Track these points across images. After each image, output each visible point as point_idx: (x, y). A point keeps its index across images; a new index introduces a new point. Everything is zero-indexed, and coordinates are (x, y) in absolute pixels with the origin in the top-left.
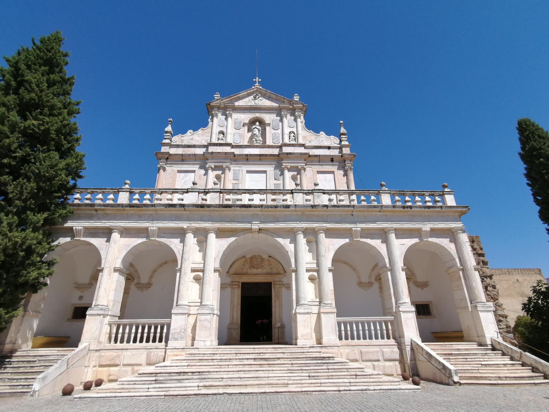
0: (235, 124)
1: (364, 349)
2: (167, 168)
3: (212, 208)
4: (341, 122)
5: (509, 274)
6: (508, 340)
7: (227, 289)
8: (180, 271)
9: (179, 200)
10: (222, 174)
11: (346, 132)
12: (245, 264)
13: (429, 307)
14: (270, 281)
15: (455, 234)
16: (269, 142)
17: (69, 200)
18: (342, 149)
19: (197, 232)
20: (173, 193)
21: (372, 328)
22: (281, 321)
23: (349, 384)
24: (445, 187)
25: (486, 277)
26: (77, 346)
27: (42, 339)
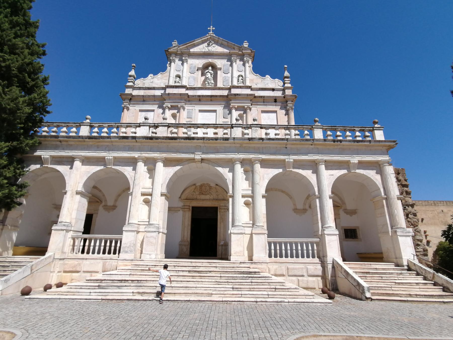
0: (190, 68)
1: (290, 266)
2: (130, 108)
3: (160, 140)
4: (286, 66)
5: (435, 205)
6: (424, 262)
7: (179, 212)
8: (131, 194)
9: (132, 133)
10: (177, 112)
11: (289, 76)
12: (195, 191)
13: (356, 232)
14: (216, 206)
15: (381, 166)
16: (220, 85)
17: (38, 132)
18: (285, 91)
19: (147, 161)
20: (127, 127)
21: (299, 248)
23: (267, 296)
24: (375, 123)
25: (408, 206)
26: (44, 254)
27: (23, 249)
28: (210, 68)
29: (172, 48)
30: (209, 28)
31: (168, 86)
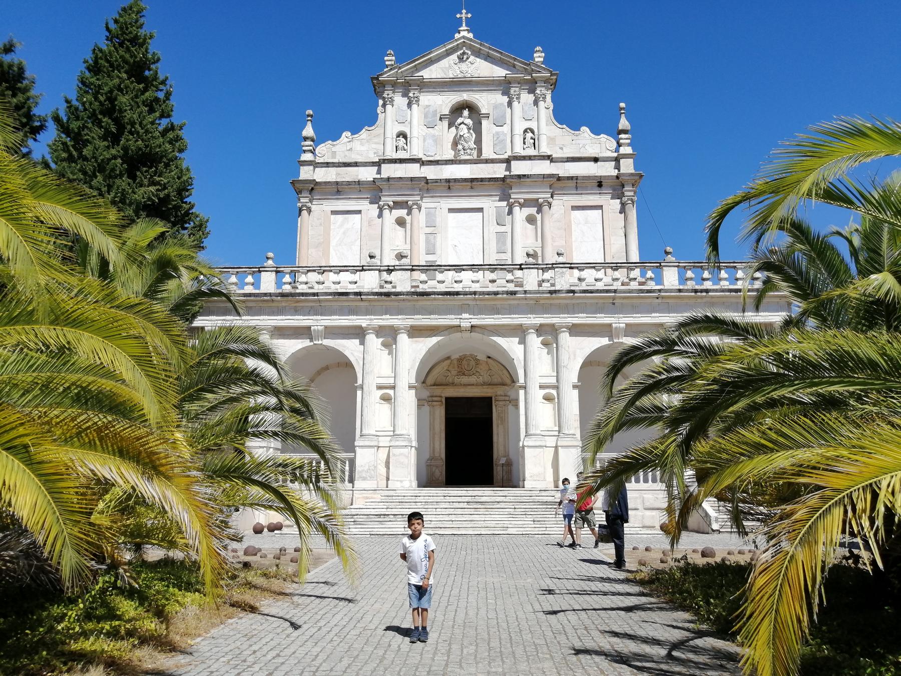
0: (426, 116)
2: (313, 208)
8: (362, 387)
10: (408, 215)
12: (450, 369)
14: (489, 395)
16: (487, 153)
22: (507, 455)
28: (466, 113)
29: (386, 72)
30: (458, 16)
31: (384, 160)
